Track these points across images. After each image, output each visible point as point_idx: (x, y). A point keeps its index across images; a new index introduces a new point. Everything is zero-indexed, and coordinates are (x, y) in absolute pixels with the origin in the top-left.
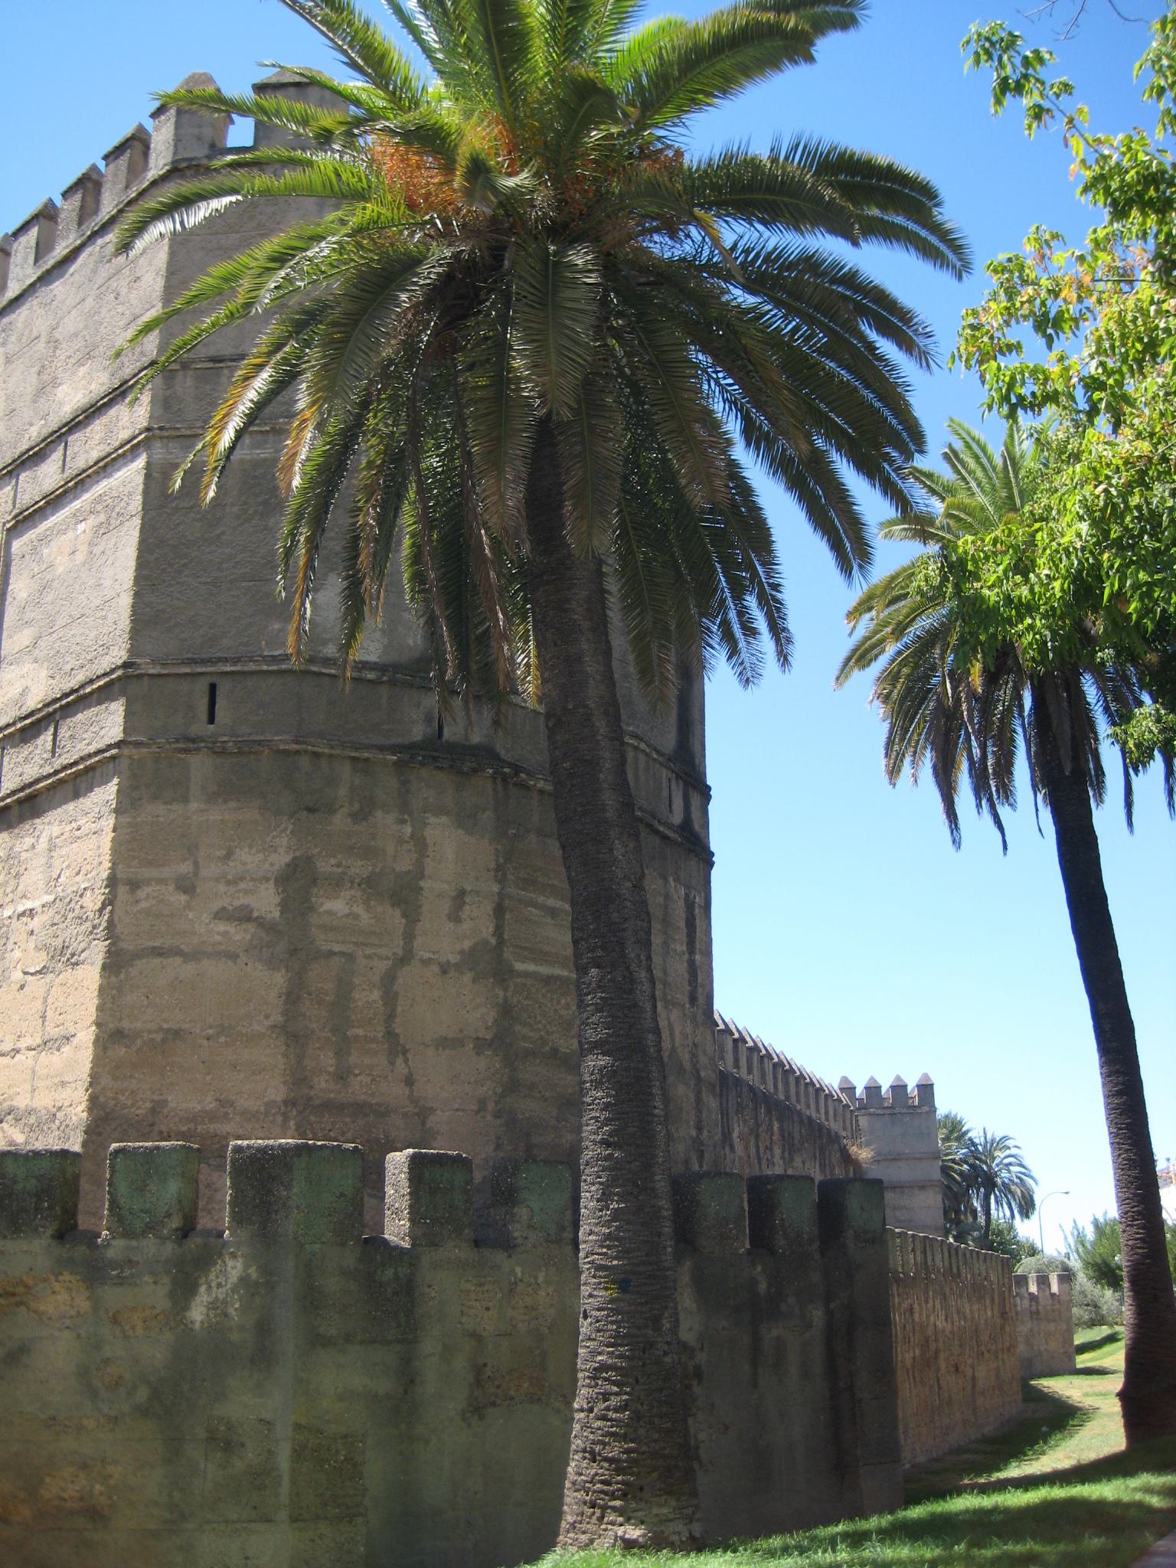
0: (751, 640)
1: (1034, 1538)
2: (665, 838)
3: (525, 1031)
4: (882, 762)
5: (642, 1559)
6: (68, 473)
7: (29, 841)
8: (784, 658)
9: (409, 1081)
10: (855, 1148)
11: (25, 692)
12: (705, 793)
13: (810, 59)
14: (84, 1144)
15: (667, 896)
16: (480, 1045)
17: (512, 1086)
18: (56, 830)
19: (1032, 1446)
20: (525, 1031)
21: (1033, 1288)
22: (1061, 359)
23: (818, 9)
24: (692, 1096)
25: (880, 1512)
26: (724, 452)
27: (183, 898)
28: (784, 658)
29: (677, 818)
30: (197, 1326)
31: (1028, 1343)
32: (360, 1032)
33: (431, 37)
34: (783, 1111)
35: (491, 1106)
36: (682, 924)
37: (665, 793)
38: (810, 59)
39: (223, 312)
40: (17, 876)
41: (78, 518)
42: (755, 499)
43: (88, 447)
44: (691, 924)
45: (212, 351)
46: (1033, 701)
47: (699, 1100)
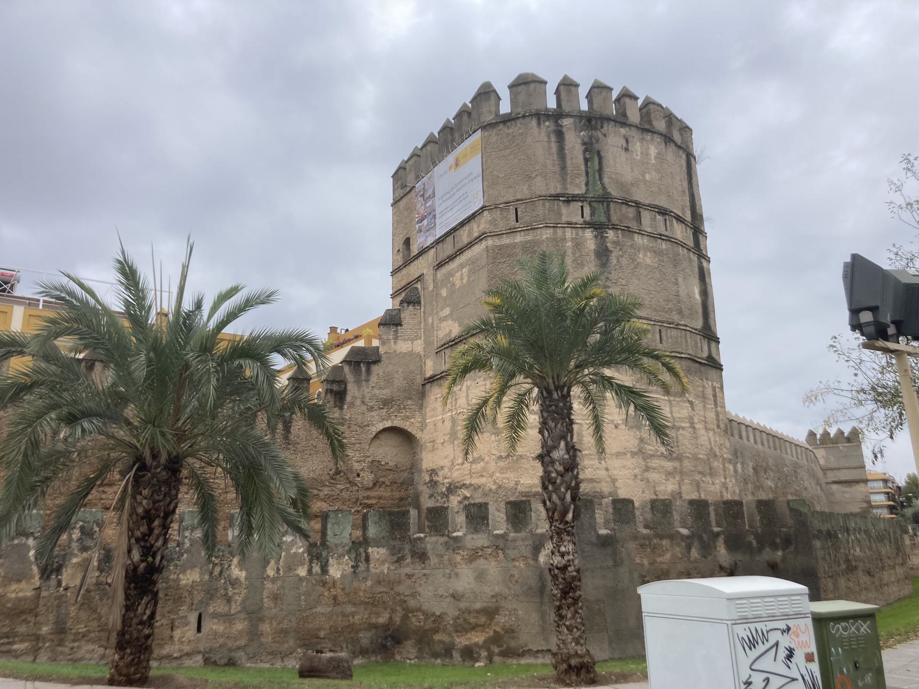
2: (701, 363)
3: (650, 447)
6: (456, 249)
7: (459, 387)
8: (264, 299)
9: (607, 469)
11: (451, 331)
12: (717, 341)
15: (704, 387)
16: (634, 454)
17: (647, 469)
18: (469, 383)
20: (650, 447)
24: (721, 466)
28: (264, 299)
29: (705, 354)
31: (691, 403)
32: (587, 452)
35: (639, 477)
36: (711, 397)
37: (699, 345)
40: (456, 399)
41: (462, 266)
43: (476, 229)
45: (505, 200)
47: (724, 466)
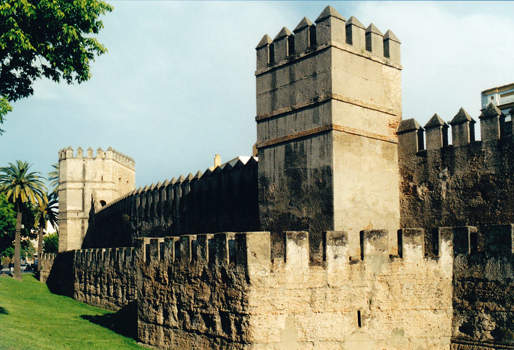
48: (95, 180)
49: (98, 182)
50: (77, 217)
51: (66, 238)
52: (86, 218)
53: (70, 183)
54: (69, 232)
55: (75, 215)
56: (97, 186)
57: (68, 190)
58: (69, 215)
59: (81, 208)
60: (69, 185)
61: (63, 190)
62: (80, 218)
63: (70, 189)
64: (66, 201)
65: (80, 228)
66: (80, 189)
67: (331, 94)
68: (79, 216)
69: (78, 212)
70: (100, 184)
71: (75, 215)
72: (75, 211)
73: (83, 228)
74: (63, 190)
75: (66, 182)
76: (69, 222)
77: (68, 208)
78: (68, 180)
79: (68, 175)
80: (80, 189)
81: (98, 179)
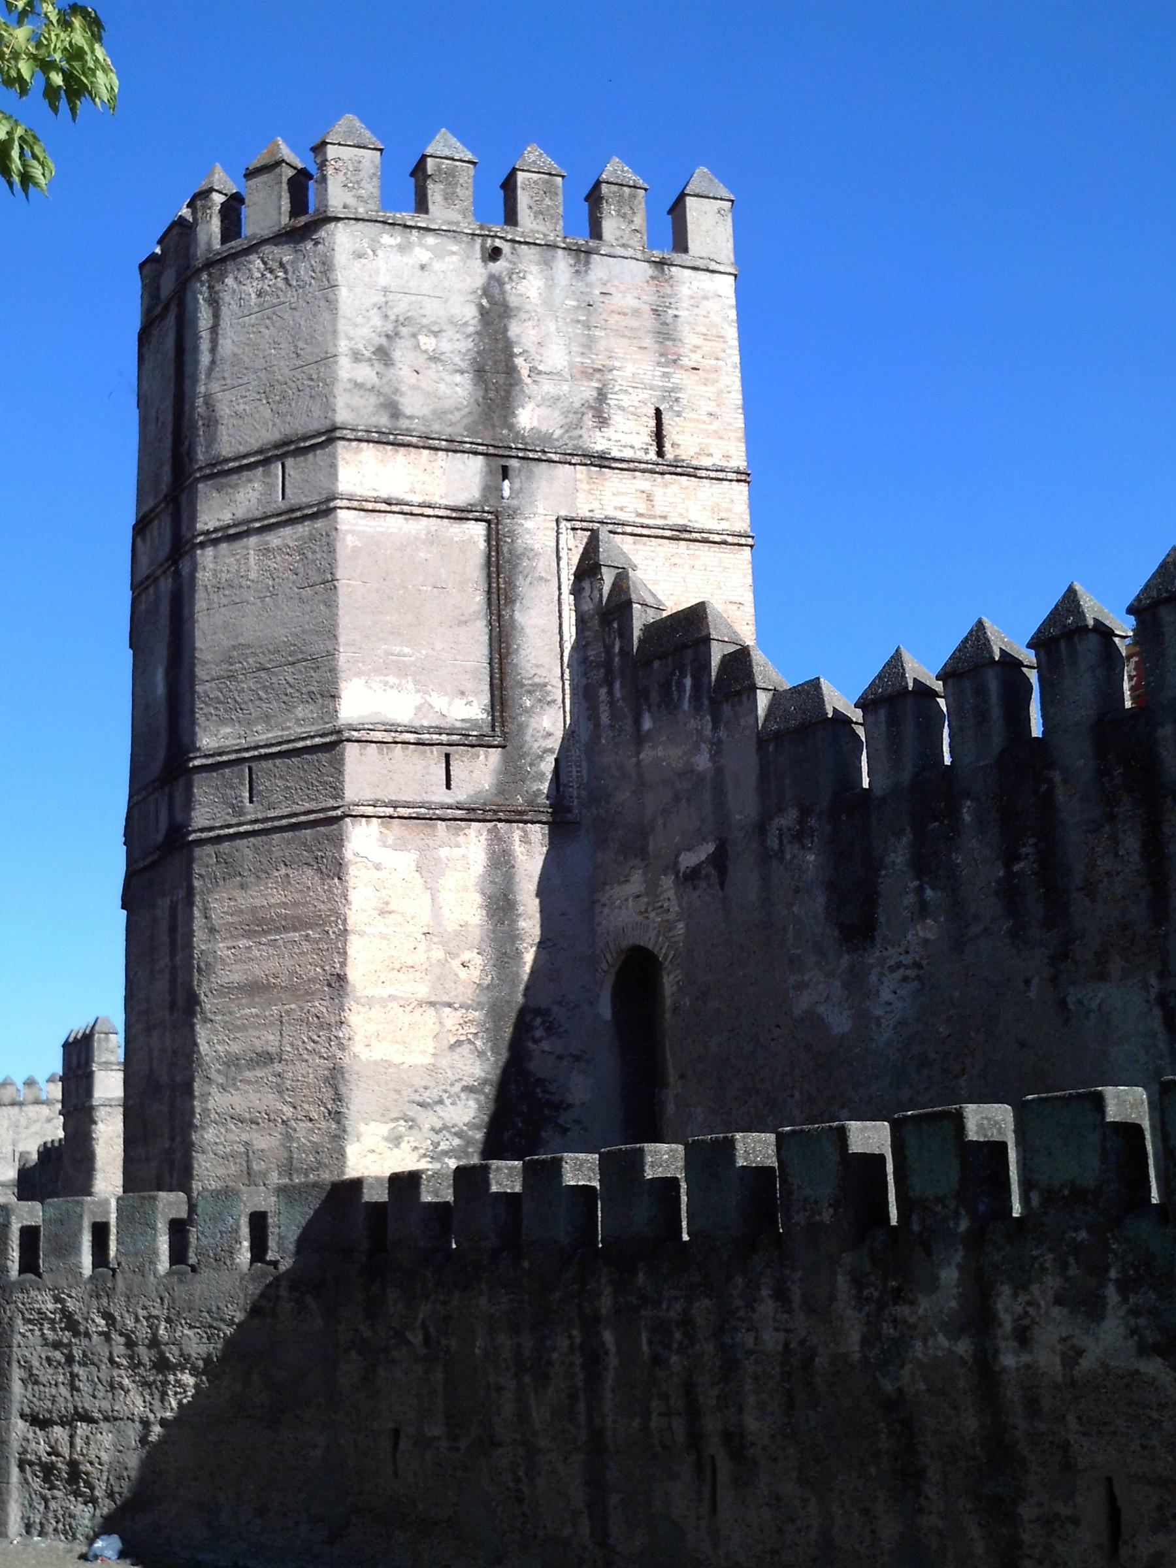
0: (382, 399)
1: (950, 1112)
4: (51, 111)
5: (481, 907)
10: (826, 1216)
13: (1130, 610)
14: (524, 1185)
19: (191, 1126)
21: (792, 980)
22: (322, 696)
23: (684, 1185)
25: (154, 1238)
26: (513, 943)
27: (786, 1316)
30: (958, 1257)
33: (568, 722)
34: (1024, 1158)
38: (1130, 610)
39: (351, 582)
42: (128, 1561)
44: (173, 929)
46: (888, 1212)
48: (599, 442)
49: (630, 466)
50: (440, 795)
51: (331, 1027)
52: (551, 751)
53: (369, 450)
54: (363, 962)
55: (417, 777)
56: (615, 496)
57: (346, 518)
58: (363, 774)
59: (472, 709)
60: (360, 471)
61: (292, 517)
62: (471, 813)
63: (365, 506)
64: (330, 632)
65: (675, 520)
66: (460, 514)
67: (326, 206)
68: (462, 793)
69: (453, 743)
70: (643, 482)
71: (417, 777)
72: (419, 739)
73: (501, 906)
74: (292, 517)
75: (330, 436)
76: (362, 840)
77: (357, 702)
78: (342, 416)
79: (346, 370)
80: (460, 514)
81: (627, 435)
